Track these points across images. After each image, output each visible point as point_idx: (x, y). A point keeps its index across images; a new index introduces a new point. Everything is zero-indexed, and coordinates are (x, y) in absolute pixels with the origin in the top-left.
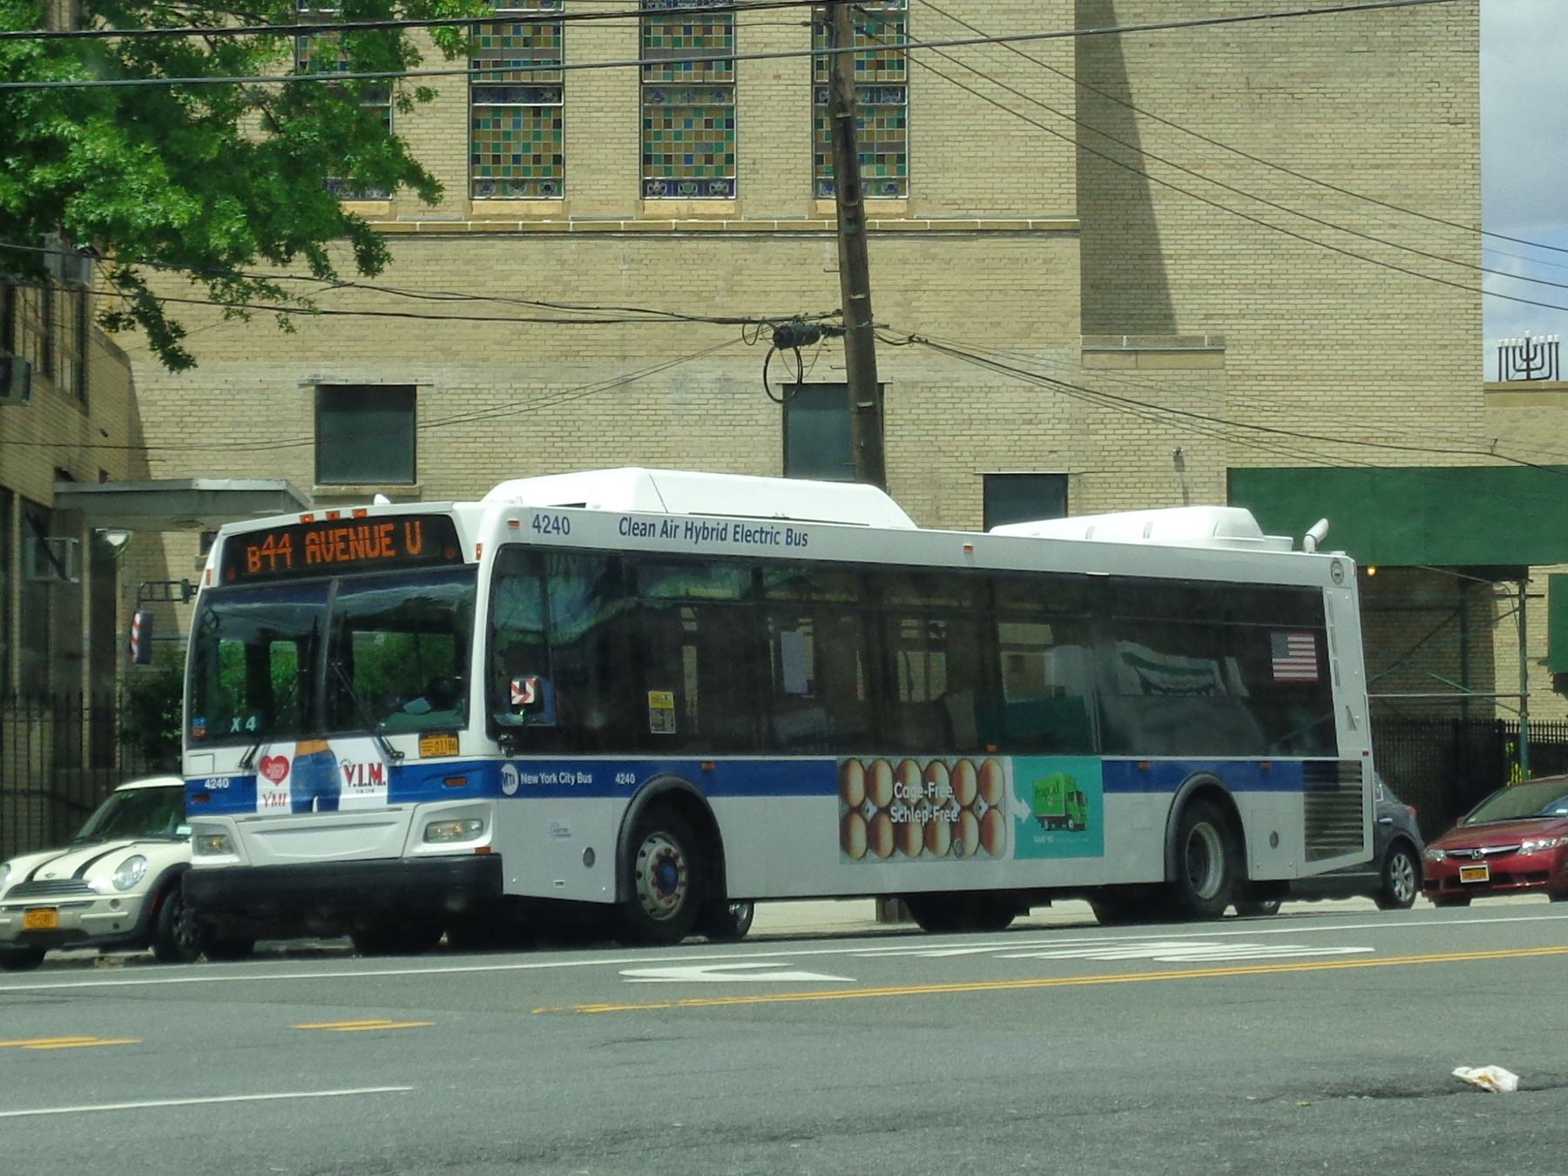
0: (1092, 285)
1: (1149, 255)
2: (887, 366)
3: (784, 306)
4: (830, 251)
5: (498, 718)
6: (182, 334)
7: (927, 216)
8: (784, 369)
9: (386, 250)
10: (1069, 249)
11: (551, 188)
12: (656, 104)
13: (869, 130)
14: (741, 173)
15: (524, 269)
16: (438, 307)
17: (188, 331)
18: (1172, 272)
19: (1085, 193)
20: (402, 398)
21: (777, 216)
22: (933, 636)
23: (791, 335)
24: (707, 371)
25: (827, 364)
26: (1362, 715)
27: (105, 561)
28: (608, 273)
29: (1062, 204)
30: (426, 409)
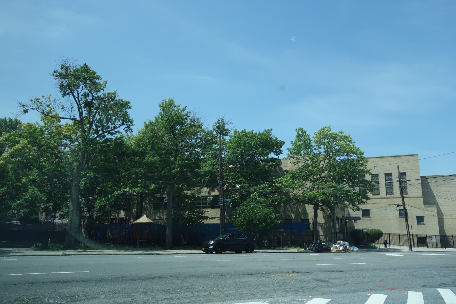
0: (424, 201)
1: (431, 193)
2: (407, 208)
3: (398, 203)
4: (401, 199)
5: (169, 239)
6: (129, 103)
7: (410, 196)
8: (398, 208)
9: (211, 128)
10: (422, 198)
11: (379, 195)
12: (387, 188)
13: (404, 190)
14: (394, 193)
15: (377, 201)
16: (370, 204)
17: (130, 101)
18: (445, 224)
19: (423, 194)
20: (369, 210)
21: (397, 196)
22: (149, 174)
23: (398, 206)
24: (393, 208)
25: (402, 208)
26: (384, 181)
27: (346, 222)
28: (384, 201)
29: (421, 195)
30: (370, 211)
